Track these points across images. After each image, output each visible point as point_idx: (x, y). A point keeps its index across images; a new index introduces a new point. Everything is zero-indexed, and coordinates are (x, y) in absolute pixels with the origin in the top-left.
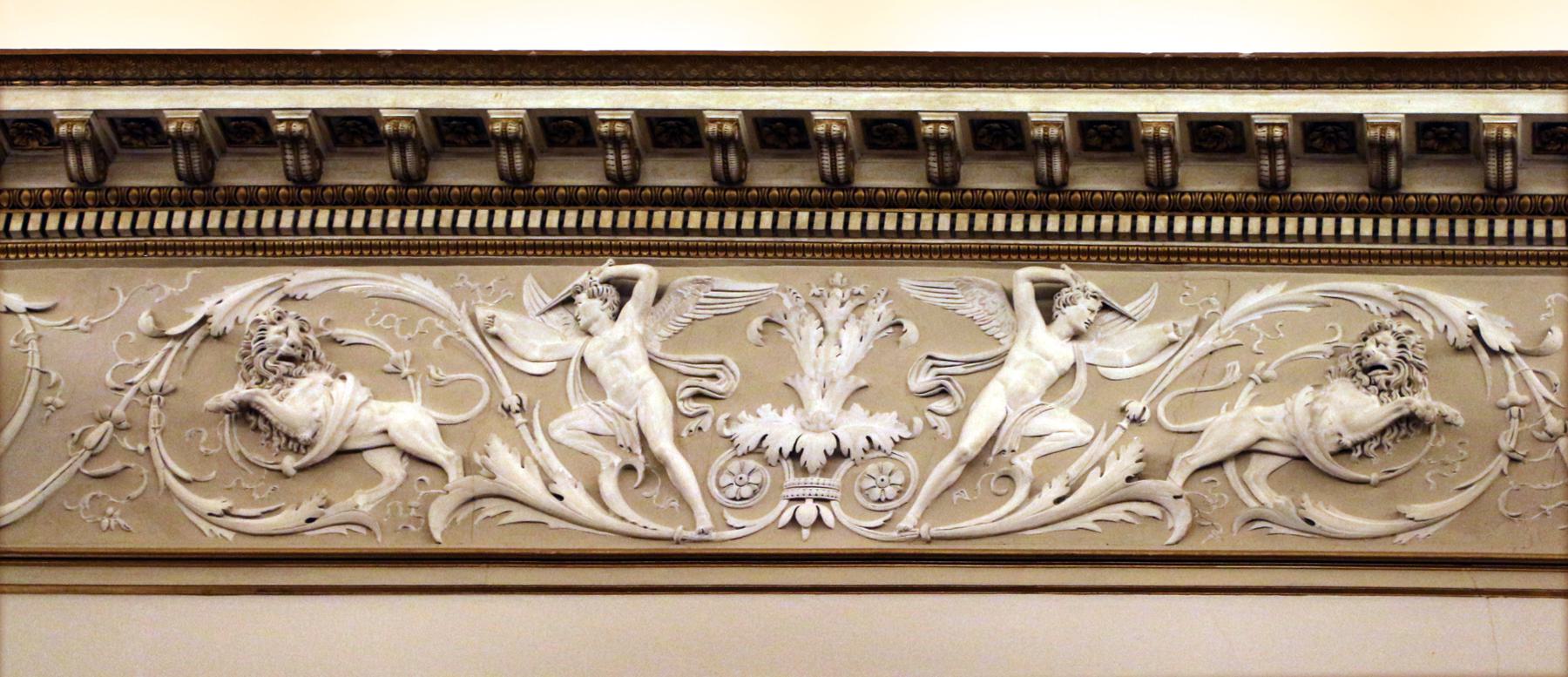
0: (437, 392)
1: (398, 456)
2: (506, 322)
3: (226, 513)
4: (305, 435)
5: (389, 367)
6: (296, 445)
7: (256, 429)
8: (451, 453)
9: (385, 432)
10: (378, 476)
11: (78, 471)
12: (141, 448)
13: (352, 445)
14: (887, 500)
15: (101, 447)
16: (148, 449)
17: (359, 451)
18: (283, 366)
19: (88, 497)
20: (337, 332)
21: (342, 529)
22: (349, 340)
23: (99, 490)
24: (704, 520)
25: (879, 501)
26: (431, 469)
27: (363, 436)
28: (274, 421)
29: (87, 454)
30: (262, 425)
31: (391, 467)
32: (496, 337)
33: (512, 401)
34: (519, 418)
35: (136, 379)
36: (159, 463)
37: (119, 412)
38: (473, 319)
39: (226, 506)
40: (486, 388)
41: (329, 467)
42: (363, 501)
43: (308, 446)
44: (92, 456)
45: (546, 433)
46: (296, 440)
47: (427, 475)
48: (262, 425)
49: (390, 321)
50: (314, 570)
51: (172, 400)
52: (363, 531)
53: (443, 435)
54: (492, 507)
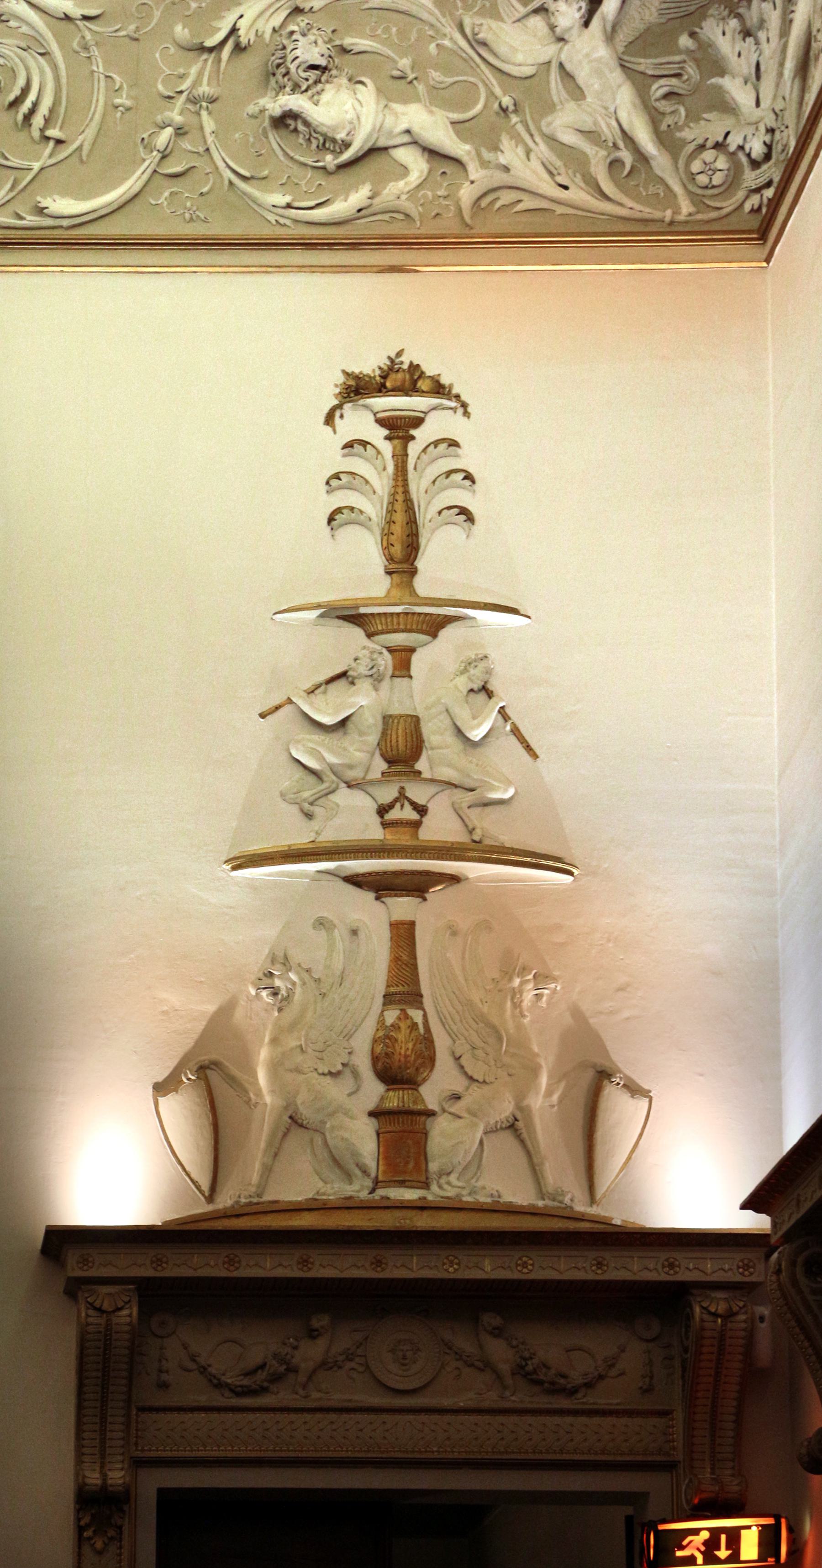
0: (438, 97)
1: (421, 151)
2: (489, 29)
3: (289, 206)
4: (341, 136)
5: (396, 73)
6: (329, 143)
7: (296, 130)
8: (467, 147)
9: (408, 132)
10: (404, 170)
11: (155, 171)
12: (201, 149)
13: (382, 143)
14: (714, 187)
15: (169, 150)
16: (208, 150)
17: (386, 149)
18: (313, 75)
19: (166, 194)
20: (348, 41)
21: (386, 217)
22: (356, 49)
23: (175, 186)
24: (686, 207)
25: (706, 187)
26: (450, 162)
27: (390, 134)
28: (314, 123)
29: (160, 155)
30: (301, 127)
31: (417, 165)
32: (484, 44)
33: (506, 101)
34: (514, 119)
35: (183, 87)
36: (221, 164)
37: (178, 119)
38: (461, 28)
39: (287, 199)
40: (481, 85)
41: (367, 160)
42: (395, 190)
43: (347, 145)
44: (164, 157)
45: (539, 130)
46: (334, 141)
47: (449, 168)
48: (301, 127)
49: (387, 30)
50: (134, 253)
51: (215, 105)
52: (401, 217)
53: (458, 133)
54: (507, 197)
